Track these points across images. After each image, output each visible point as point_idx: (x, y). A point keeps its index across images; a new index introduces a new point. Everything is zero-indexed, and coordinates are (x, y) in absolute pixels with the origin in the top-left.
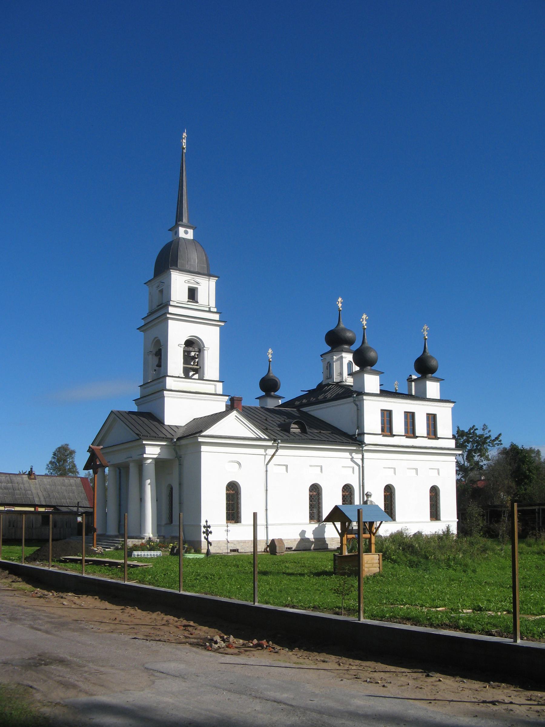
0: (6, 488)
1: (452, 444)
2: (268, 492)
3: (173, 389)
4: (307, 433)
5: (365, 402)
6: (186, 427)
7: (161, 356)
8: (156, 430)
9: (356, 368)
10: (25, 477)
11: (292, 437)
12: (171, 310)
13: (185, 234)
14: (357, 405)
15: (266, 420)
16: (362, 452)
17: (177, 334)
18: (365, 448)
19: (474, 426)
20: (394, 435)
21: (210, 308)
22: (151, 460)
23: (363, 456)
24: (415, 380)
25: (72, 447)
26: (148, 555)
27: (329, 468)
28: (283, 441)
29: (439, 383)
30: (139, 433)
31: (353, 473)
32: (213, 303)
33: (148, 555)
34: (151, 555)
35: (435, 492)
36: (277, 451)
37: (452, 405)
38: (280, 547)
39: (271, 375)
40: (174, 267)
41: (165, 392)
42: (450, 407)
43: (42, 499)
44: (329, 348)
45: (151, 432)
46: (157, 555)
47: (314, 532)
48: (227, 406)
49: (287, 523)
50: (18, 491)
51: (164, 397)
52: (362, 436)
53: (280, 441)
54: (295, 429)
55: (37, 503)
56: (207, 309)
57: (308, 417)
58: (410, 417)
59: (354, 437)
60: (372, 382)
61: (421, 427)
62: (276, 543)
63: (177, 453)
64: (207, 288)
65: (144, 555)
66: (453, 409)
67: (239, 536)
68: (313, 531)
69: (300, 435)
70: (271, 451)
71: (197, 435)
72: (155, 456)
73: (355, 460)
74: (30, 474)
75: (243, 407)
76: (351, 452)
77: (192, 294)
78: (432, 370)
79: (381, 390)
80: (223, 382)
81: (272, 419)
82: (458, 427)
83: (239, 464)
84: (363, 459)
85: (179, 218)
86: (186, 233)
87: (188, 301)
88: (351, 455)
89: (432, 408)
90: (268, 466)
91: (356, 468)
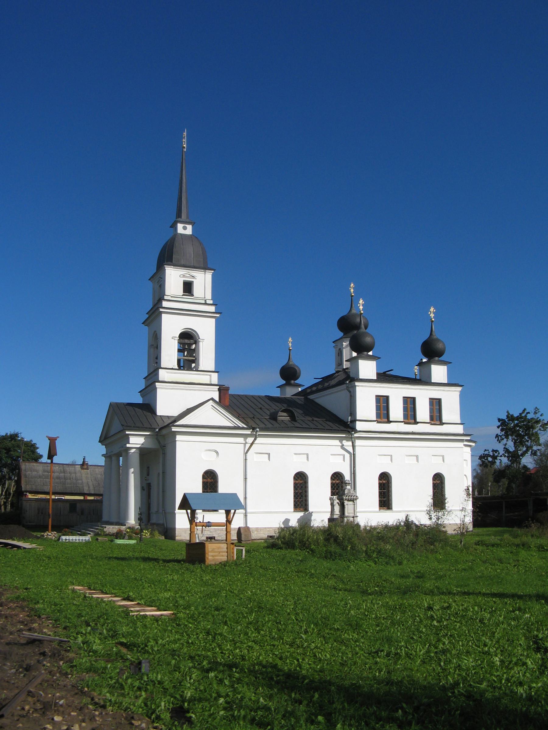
0: (58, 478)
2: (248, 480)
3: (166, 380)
4: (295, 421)
5: (358, 389)
10: (78, 468)
12: (165, 304)
13: (184, 230)
14: (350, 392)
15: (261, 409)
16: (353, 440)
17: (171, 327)
18: (356, 435)
19: (525, 410)
20: (391, 422)
21: (206, 300)
22: (135, 450)
26: (76, 540)
27: (319, 455)
28: (262, 429)
31: (344, 460)
32: (209, 296)
33: (76, 540)
34: (79, 540)
36: (255, 439)
37: (459, 389)
38: (245, 535)
39: (291, 363)
40: (169, 263)
41: (157, 384)
42: (344, 389)
43: (92, 488)
44: (341, 334)
46: (85, 540)
47: (299, 521)
49: (268, 512)
50: (69, 481)
51: (156, 388)
54: (283, 417)
55: (85, 492)
56: (203, 302)
58: (410, 404)
60: (367, 368)
64: (203, 281)
65: (72, 540)
66: (461, 392)
68: (298, 519)
70: (250, 440)
72: (138, 446)
73: (345, 447)
74: (84, 465)
75: (233, 396)
76: (341, 439)
77: (188, 287)
78: (439, 354)
79: (378, 374)
80: (218, 372)
82: (508, 412)
83: (217, 453)
84: (354, 446)
85: (179, 215)
86: (185, 228)
87: (183, 295)
88: (341, 443)
90: (248, 454)
91: (347, 456)
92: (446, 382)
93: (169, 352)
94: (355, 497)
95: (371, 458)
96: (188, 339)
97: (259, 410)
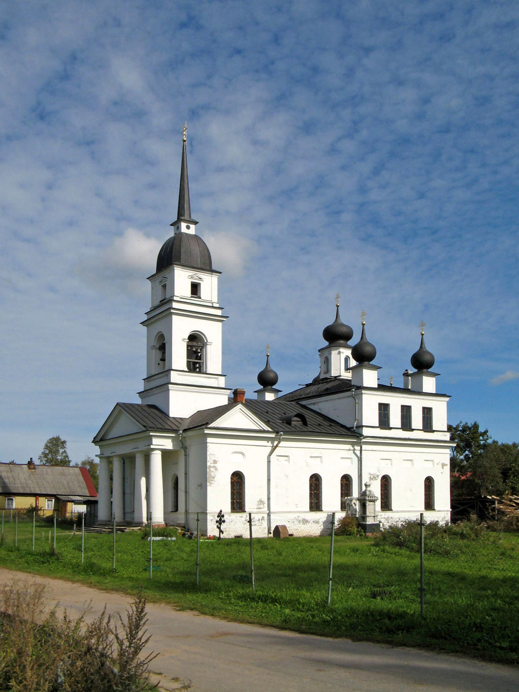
1: (447, 436)
4: (307, 426)
6: (190, 419)
7: (165, 349)
8: (160, 421)
9: (353, 363)
11: (293, 429)
12: (175, 305)
15: (267, 413)
16: (360, 444)
17: (181, 329)
18: (363, 440)
23: (361, 447)
24: (411, 375)
25: (63, 438)
27: (331, 459)
28: (286, 433)
29: (434, 379)
30: (147, 425)
32: (215, 299)
35: (429, 483)
36: (279, 442)
37: (447, 399)
40: (177, 263)
42: (445, 401)
44: (326, 343)
45: (157, 423)
48: (229, 399)
51: (169, 390)
52: (361, 428)
53: (282, 433)
57: (307, 412)
58: (406, 411)
59: (352, 430)
61: (417, 421)
62: (280, 528)
63: (182, 444)
66: (448, 403)
67: (235, 526)
69: (301, 427)
71: (204, 427)
76: (353, 444)
77: (195, 288)
79: (379, 385)
81: (273, 412)
83: (242, 453)
84: (361, 450)
86: (188, 227)
87: (192, 297)
89: (428, 402)
92: (435, 392)
93: (179, 356)
94: (376, 498)
95: (377, 461)
96: (196, 343)
97: (266, 414)
